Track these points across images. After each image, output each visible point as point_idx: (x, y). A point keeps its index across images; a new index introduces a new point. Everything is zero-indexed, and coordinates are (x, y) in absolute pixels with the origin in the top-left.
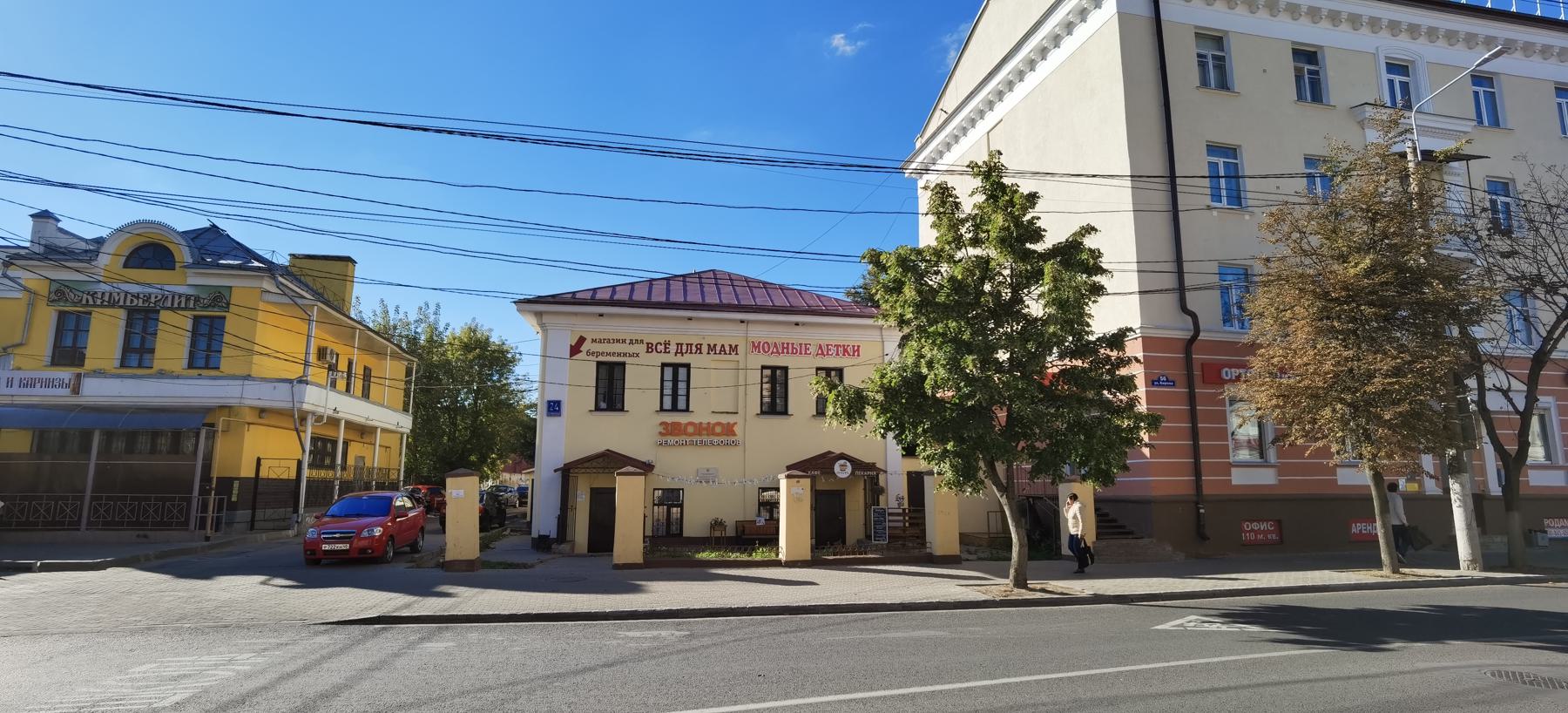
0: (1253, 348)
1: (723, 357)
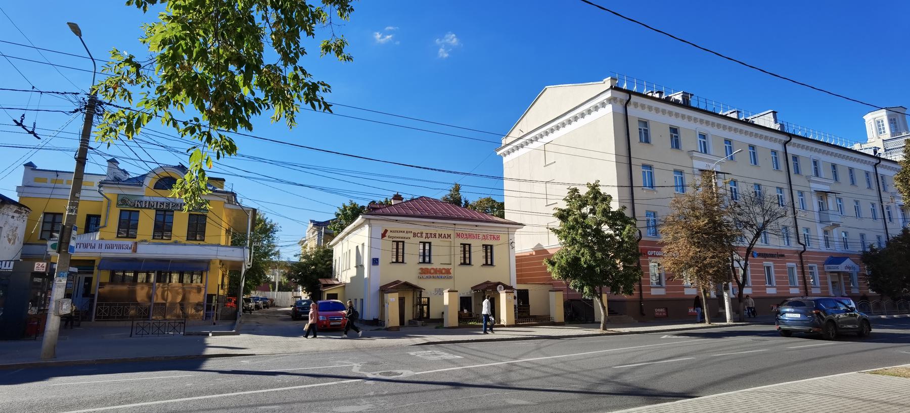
0: (663, 244)
1: (445, 239)
